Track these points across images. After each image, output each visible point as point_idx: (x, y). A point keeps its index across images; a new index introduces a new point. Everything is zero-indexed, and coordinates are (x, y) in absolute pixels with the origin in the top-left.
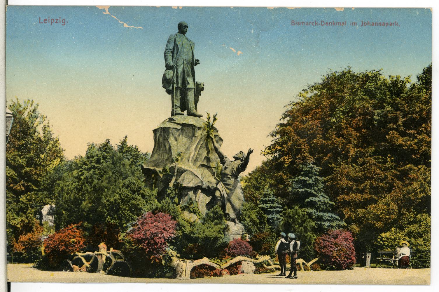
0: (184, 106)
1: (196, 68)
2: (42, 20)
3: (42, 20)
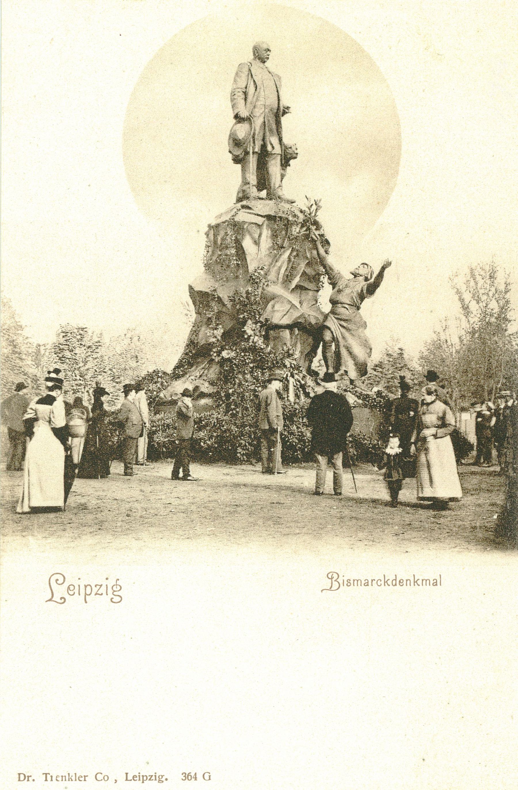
0: (263, 182)
1: (284, 120)
2: (130, 777)
3: (130, 777)
